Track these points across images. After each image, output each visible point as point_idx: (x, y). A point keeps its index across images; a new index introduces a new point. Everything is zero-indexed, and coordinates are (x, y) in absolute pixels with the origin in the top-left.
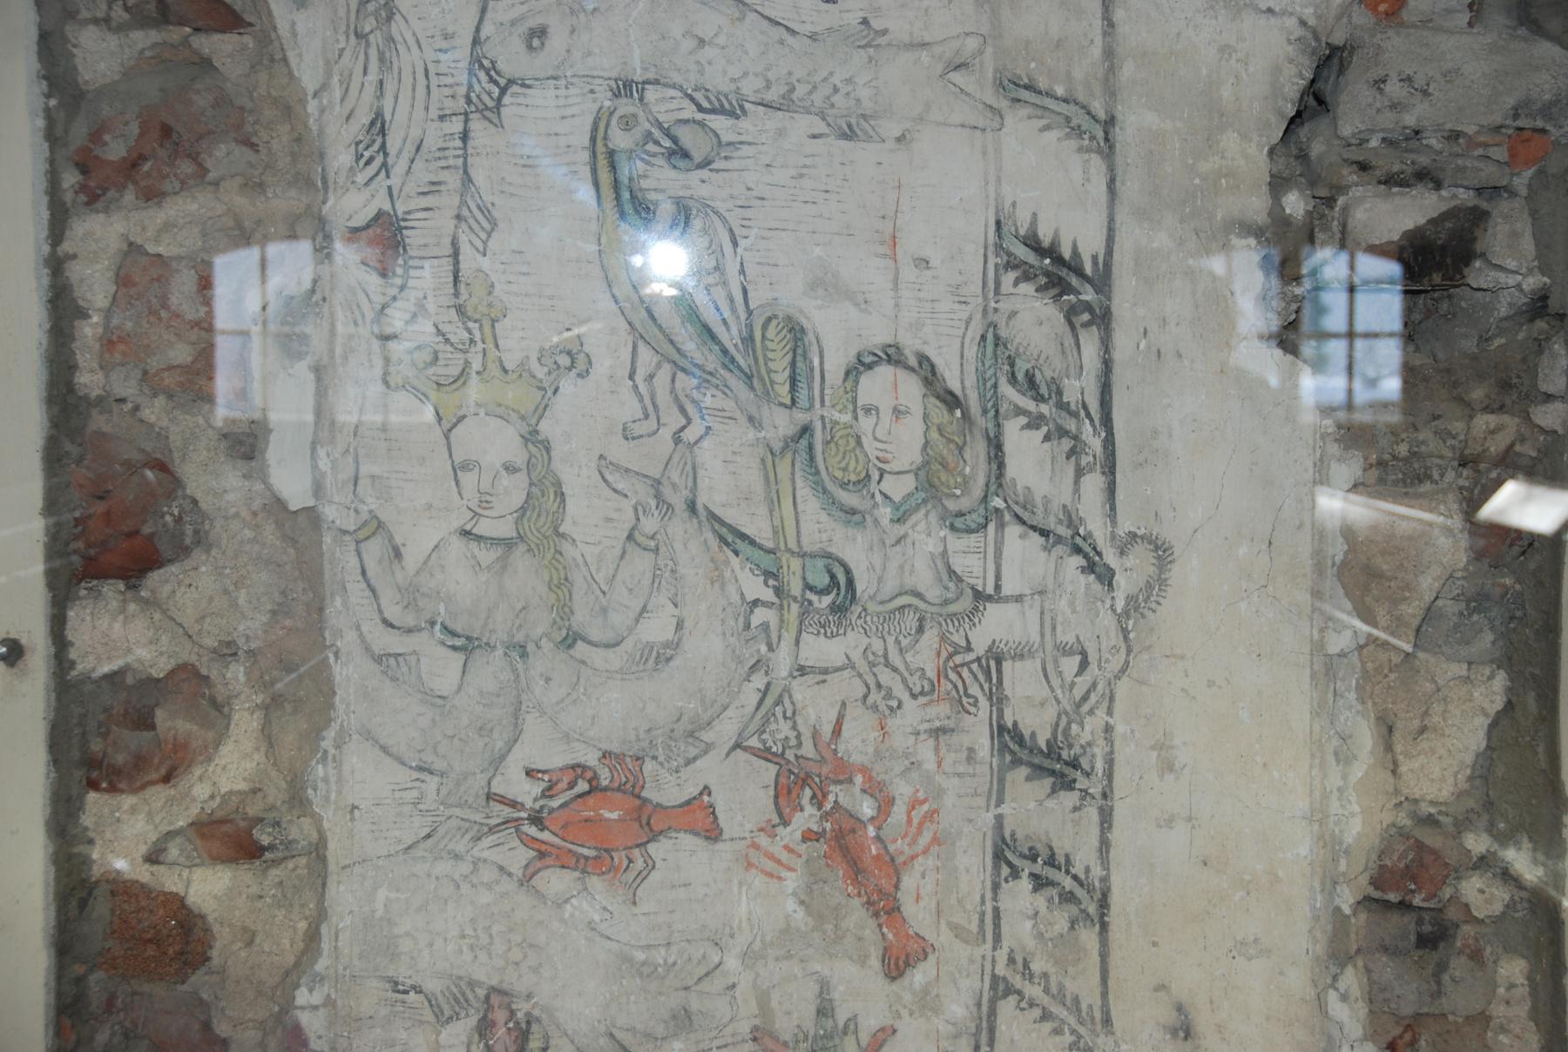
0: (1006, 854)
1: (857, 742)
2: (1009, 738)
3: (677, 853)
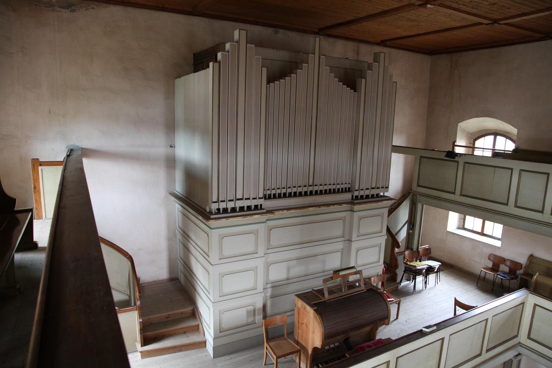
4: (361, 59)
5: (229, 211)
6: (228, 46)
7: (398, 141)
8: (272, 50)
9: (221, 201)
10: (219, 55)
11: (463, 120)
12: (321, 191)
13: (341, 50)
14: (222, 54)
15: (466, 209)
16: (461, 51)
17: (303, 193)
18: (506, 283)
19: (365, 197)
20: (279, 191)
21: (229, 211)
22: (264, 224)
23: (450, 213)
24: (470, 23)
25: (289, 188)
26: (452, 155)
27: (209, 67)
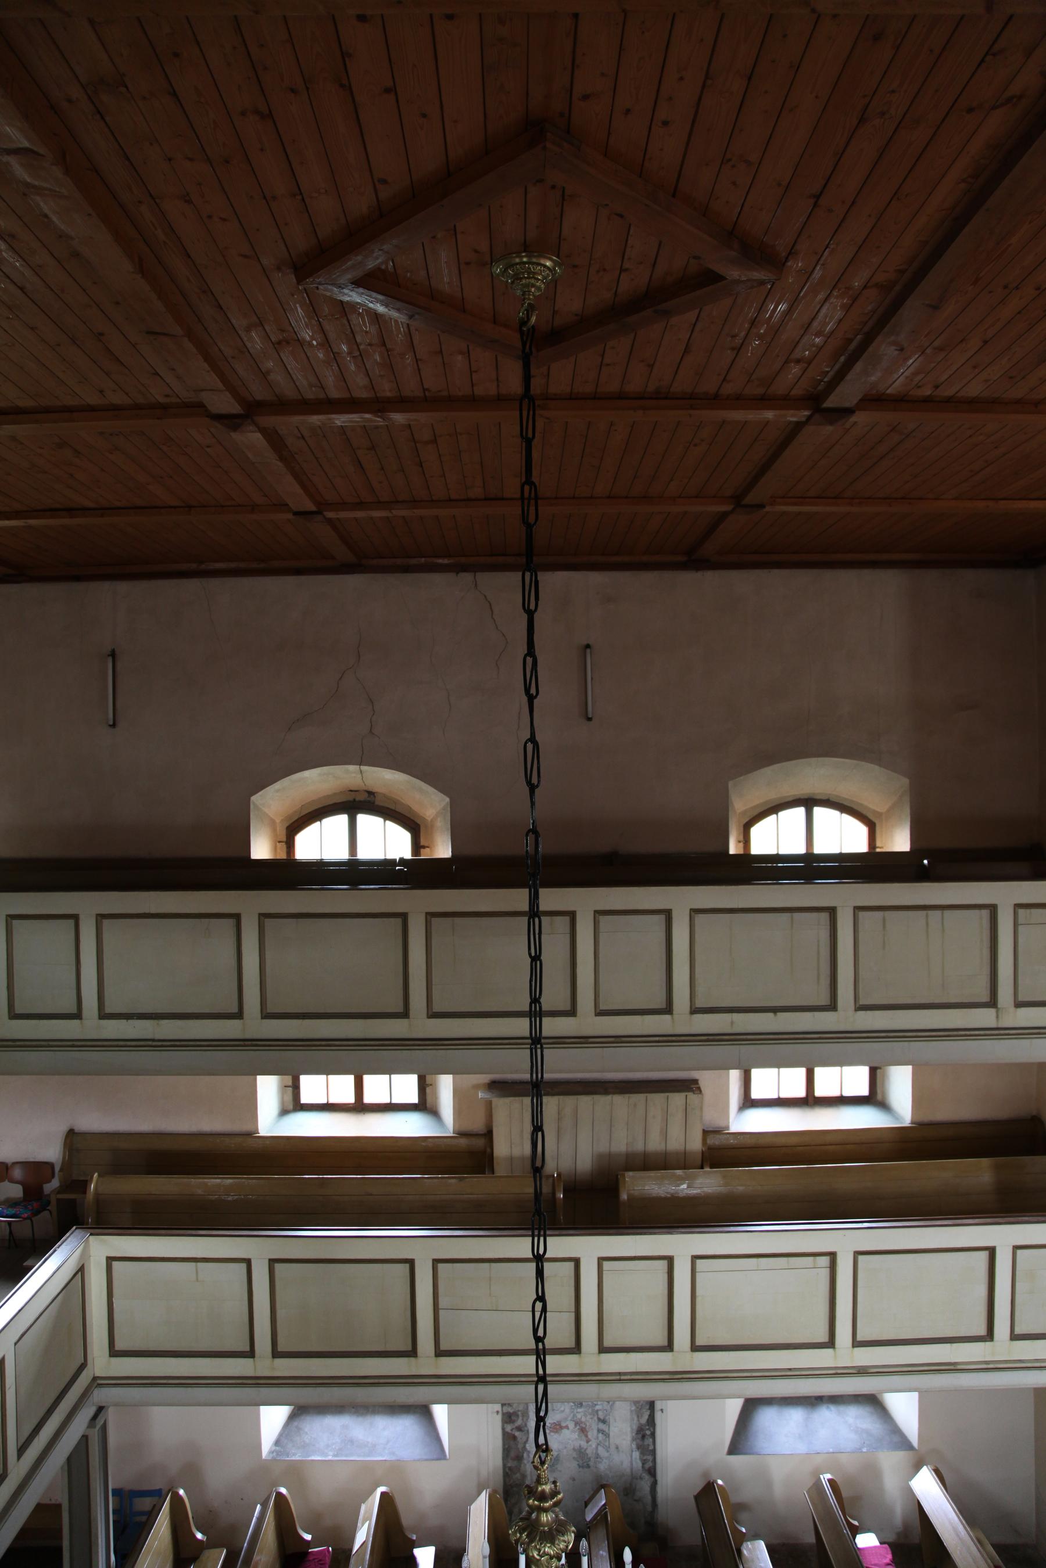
0: (599, 1431)
1: (583, 1419)
2: (599, 1419)
3: (565, 1431)
15: (294, 1057)
18: (24, 1231)
23: (258, 1077)
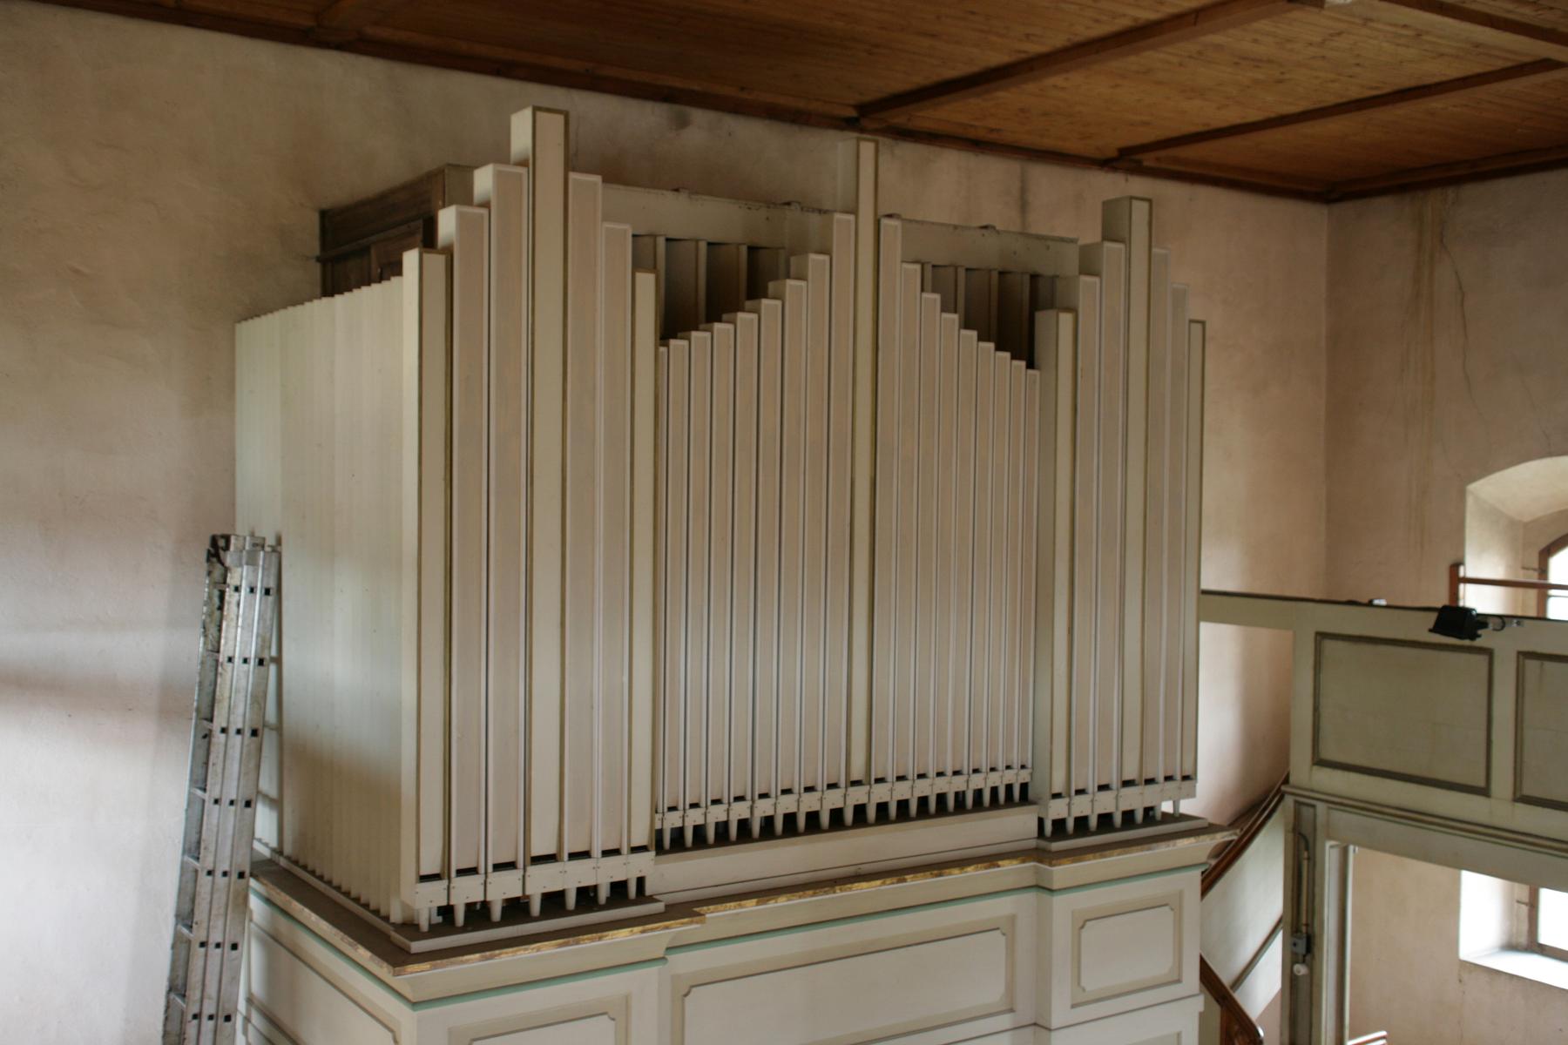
4: (1039, 226)
5: (496, 913)
6: (484, 180)
7: (1221, 570)
8: (670, 195)
9: (461, 872)
10: (447, 222)
11: (1487, 470)
12: (903, 805)
13: (953, 193)
14: (461, 217)
16: (1458, 181)
17: (825, 819)
19: (1093, 822)
20: (717, 814)
21: (496, 913)
22: (654, 970)
24: (1501, 64)
25: (764, 796)
26: (1458, 623)
27: (399, 273)
